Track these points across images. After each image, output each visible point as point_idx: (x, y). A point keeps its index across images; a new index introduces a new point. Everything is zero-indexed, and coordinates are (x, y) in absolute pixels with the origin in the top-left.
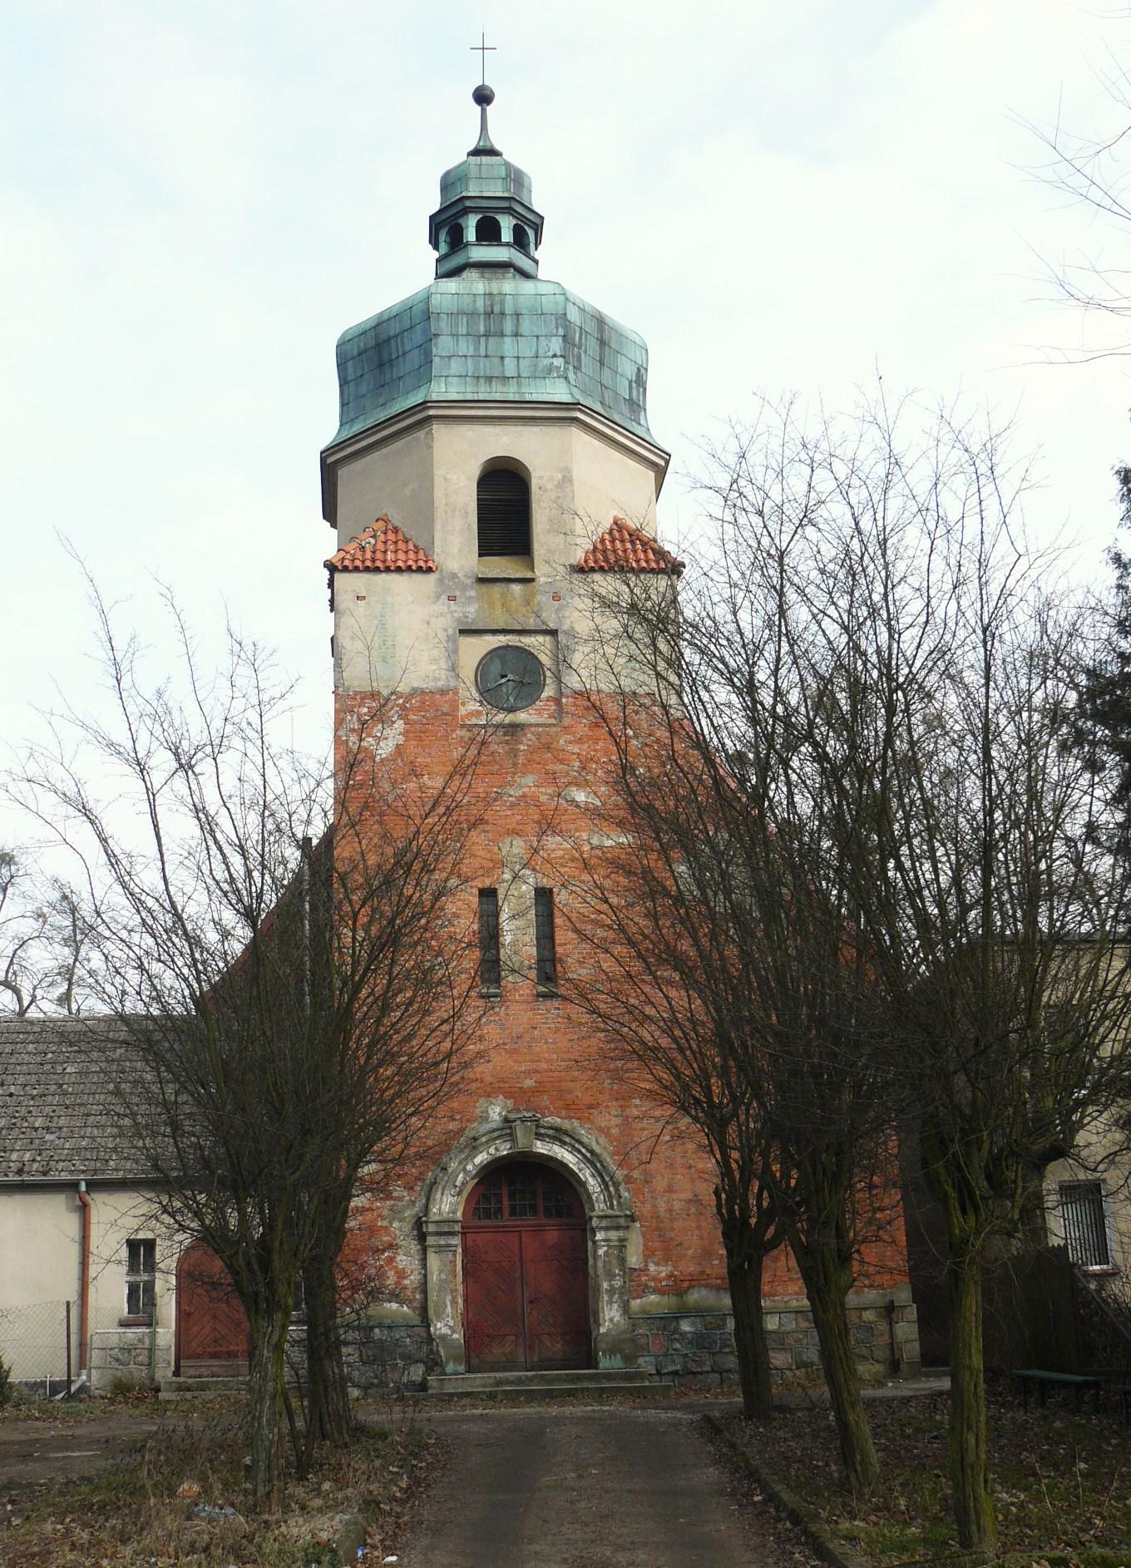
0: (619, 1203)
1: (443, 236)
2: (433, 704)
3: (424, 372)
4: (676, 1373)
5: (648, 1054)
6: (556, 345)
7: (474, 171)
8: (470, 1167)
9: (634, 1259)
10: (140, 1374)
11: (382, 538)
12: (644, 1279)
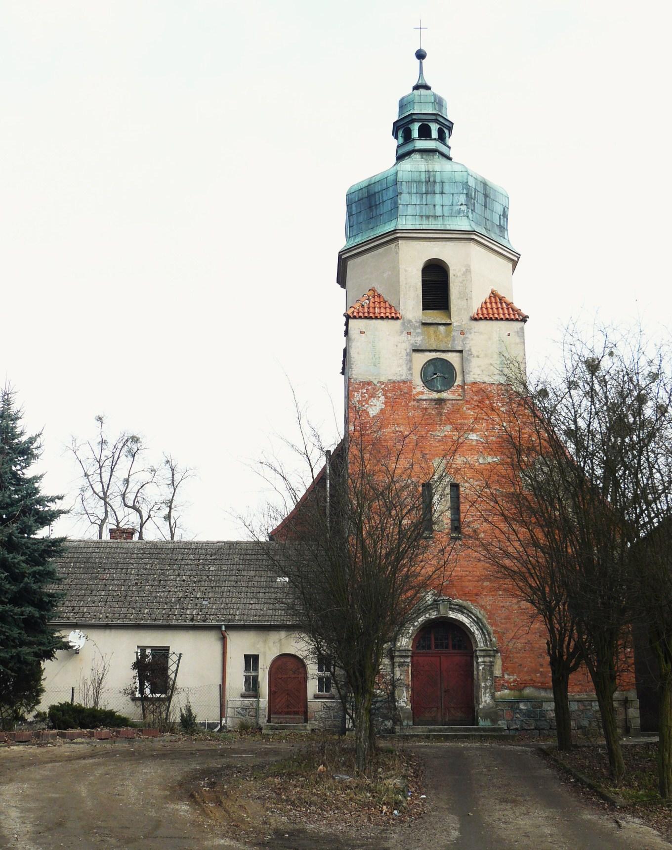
1: (400, 134)
2: (399, 388)
3: (394, 213)
4: (517, 729)
5: (511, 574)
6: (462, 199)
7: (417, 99)
9: (498, 672)
10: (251, 721)
11: (372, 300)
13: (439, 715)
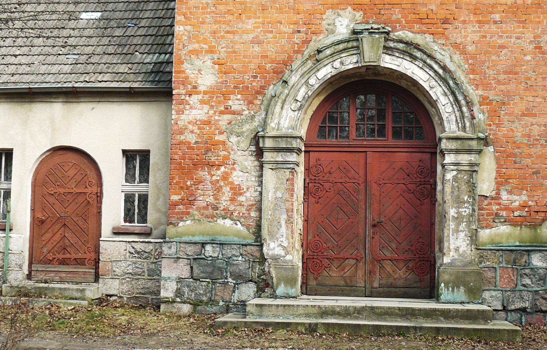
0: (473, 125)
4: (523, 310)
8: (312, 81)
9: (486, 185)
12: (495, 208)
13: (360, 273)
